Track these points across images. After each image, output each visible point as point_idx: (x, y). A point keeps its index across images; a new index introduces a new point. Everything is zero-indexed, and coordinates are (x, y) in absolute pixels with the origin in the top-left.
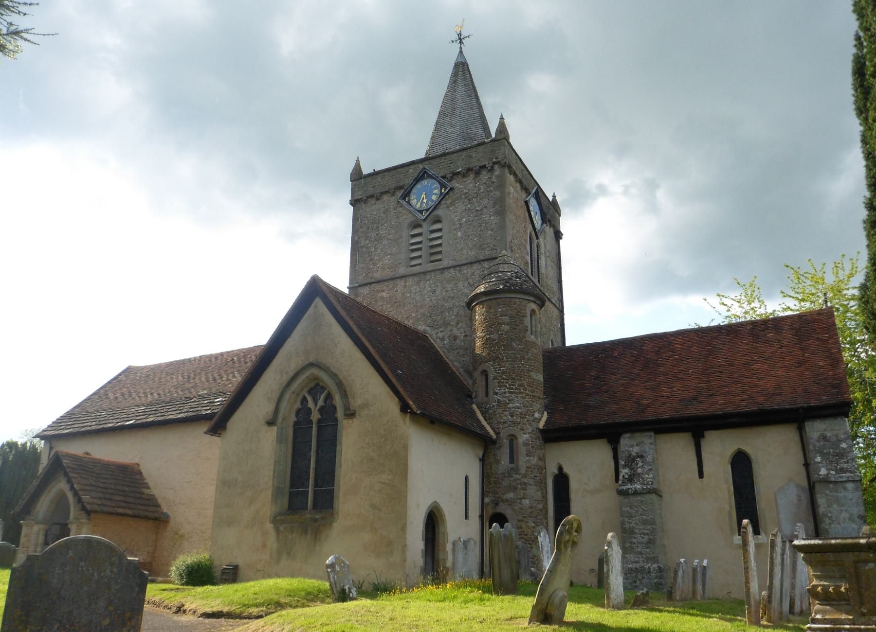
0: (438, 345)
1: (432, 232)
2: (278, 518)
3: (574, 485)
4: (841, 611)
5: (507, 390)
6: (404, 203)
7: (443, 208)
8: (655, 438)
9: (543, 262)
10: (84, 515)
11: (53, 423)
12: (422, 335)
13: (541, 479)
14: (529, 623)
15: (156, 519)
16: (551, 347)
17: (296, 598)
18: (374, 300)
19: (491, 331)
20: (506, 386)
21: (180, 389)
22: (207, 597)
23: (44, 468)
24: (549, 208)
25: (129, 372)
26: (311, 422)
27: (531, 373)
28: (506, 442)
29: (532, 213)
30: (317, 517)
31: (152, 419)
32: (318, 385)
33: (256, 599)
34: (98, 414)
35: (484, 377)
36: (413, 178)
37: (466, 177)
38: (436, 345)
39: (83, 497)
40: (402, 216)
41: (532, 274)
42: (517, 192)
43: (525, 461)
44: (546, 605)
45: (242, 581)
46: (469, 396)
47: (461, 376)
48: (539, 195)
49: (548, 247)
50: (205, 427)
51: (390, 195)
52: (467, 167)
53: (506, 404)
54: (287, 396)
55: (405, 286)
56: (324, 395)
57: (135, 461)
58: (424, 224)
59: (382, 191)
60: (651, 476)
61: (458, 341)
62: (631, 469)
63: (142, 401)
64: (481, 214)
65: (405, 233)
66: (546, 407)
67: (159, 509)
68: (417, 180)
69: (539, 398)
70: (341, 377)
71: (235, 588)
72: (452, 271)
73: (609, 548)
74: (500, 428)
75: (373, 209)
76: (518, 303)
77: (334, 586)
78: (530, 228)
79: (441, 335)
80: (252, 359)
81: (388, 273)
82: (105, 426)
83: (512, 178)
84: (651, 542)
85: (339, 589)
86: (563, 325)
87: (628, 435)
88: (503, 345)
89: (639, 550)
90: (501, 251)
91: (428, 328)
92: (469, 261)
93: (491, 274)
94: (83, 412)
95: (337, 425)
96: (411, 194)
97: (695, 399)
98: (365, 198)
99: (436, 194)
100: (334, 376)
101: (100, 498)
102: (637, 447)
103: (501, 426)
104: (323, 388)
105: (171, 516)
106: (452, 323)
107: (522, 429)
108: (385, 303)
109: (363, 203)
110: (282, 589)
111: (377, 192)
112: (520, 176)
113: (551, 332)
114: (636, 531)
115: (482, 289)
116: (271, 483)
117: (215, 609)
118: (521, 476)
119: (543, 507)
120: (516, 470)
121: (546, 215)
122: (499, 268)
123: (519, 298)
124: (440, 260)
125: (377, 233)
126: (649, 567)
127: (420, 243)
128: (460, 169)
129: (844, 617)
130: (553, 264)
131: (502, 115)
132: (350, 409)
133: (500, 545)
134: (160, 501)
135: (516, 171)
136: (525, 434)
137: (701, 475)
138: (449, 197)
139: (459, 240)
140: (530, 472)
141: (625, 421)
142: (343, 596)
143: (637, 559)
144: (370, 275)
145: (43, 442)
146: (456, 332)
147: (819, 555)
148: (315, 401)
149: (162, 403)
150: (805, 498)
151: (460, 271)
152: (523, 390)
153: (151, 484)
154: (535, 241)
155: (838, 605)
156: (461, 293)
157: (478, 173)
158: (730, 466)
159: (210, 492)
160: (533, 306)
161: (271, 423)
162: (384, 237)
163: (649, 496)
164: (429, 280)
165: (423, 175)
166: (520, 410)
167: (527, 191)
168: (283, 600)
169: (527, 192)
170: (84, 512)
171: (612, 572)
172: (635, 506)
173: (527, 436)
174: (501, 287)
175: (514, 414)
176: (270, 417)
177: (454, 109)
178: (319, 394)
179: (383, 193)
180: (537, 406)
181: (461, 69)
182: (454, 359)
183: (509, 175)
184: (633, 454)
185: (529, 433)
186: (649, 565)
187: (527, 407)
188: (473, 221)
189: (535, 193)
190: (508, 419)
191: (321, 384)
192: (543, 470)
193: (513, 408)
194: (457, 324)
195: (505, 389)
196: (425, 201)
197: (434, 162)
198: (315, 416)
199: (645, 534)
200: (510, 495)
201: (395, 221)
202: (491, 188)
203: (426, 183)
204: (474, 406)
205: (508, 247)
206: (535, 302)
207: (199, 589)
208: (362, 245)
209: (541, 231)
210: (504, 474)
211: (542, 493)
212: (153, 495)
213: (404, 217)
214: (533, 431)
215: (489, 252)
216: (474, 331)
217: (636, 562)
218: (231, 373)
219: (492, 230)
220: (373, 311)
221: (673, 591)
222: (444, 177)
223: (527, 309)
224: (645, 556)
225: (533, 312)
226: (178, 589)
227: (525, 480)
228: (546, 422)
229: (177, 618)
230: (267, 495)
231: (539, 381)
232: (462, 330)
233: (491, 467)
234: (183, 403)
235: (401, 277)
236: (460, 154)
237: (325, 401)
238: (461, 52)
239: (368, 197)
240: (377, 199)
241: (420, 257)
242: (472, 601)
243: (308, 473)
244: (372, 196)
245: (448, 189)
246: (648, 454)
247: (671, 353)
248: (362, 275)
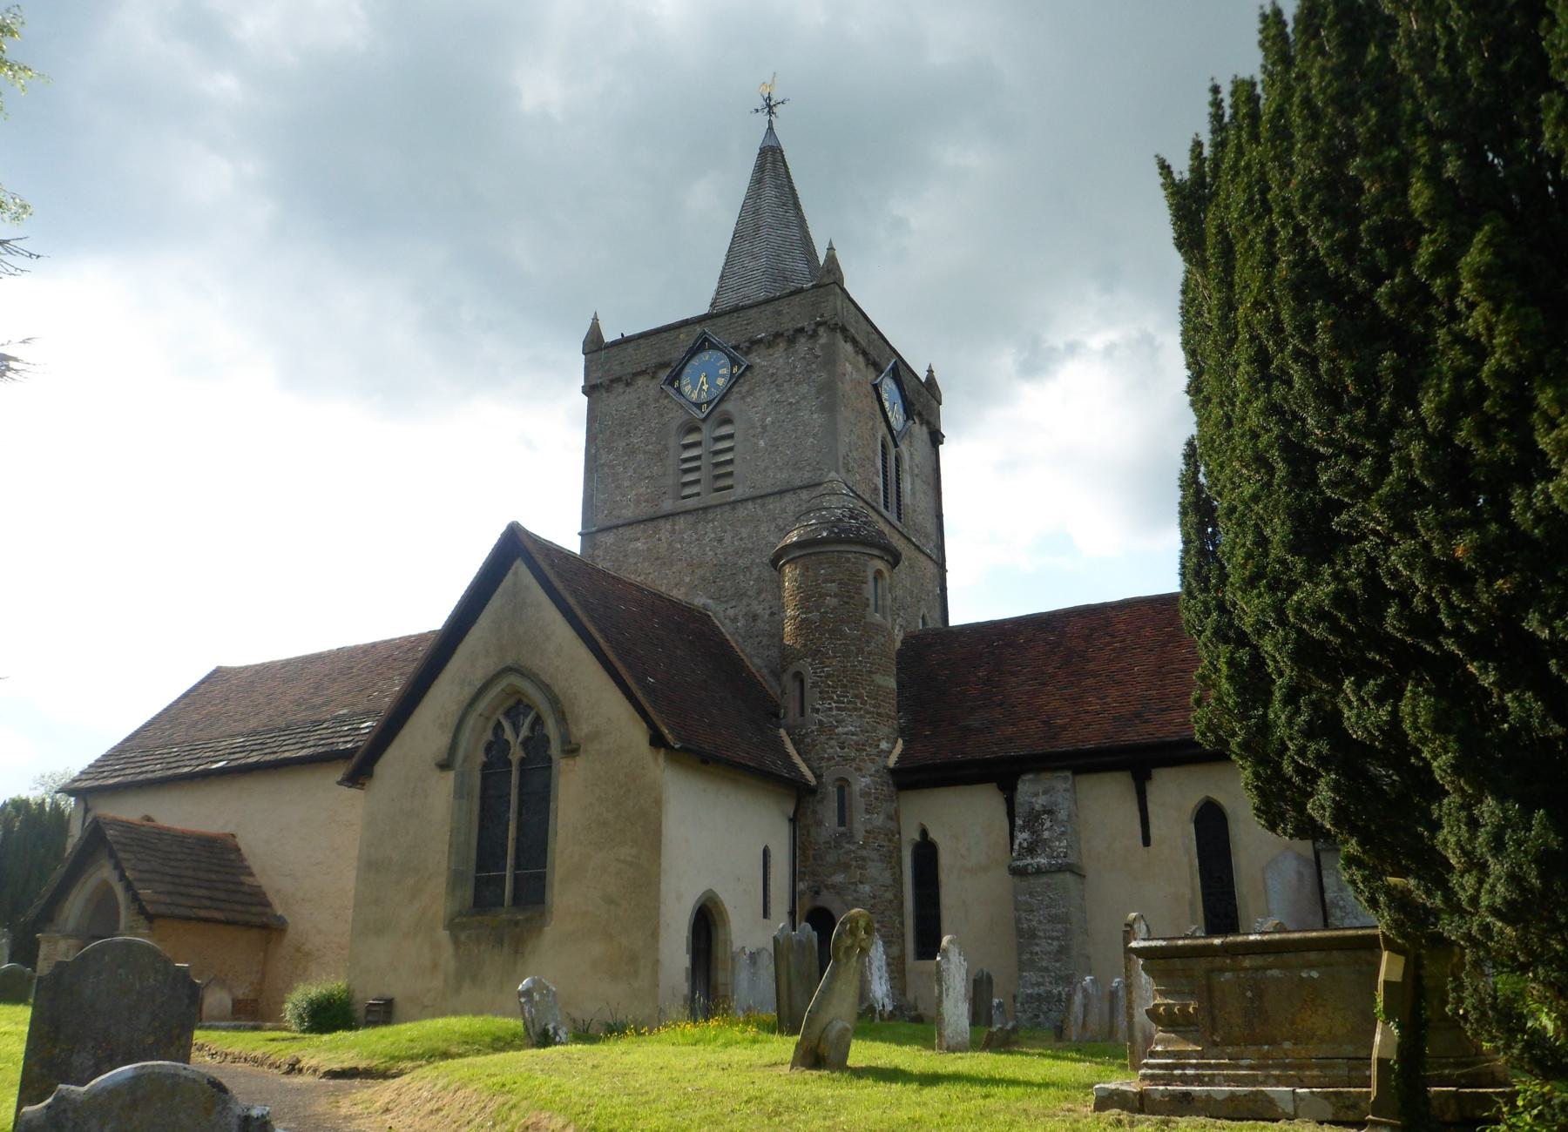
0: (726, 630)
3: (945, 860)
4: (1188, 1040)
5: (834, 705)
6: (672, 392)
9: (906, 485)
10: (142, 920)
11: (90, 766)
12: (700, 613)
13: (890, 851)
14: (791, 1069)
15: (264, 927)
17: (477, 1046)
19: (807, 608)
20: (832, 698)
21: (303, 707)
22: (337, 1048)
23: (75, 846)
24: (919, 394)
25: (218, 676)
26: (509, 763)
28: (832, 790)
29: (887, 405)
30: (520, 917)
31: (255, 759)
32: (519, 702)
33: (412, 1048)
34: (165, 751)
36: (687, 349)
38: (723, 630)
39: (141, 891)
40: (667, 414)
41: (886, 507)
42: (858, 370)
44: (816, 1042)
45: (400, 1022)
46: (773, 713)
47: (765, 680)
48: (900, 371)
49: (918, 459)
50: (339, 772)
51: (647, 377)
54: (471, 721)
55: (673, 532)
56: (530, 718)
57: (227, 830)
58: (704, 427)
61: (759, 623)
62: (1033, 833)
63: (240, 727)
65: (673, 442)
66: (902, 732)
67: (268, 910)
68: (693, 352)
69: (889, 717)
70: (556, 690)
71: (381, 1033)
72: (750, 505)
73: (942, 958)
75: (620, 401)
77: (530, 1026)
78: (882, 430)
79: (731, 612)
82: (177, 771)
83: (849, 347)
84: (1063, 951)
85: (537, 1028)
86: (944, 589)
87: (1031, 776)
90: (829, 471)
91: (710, 601)
92: (776, 490)
93: (809, 512)
94: (140, 747)
95: (551, 767)
96: (683, 377)
97: (1138, 715)
99: (723, 376)
100: (546, 688)
101: (169, 893)
104: (529, 708)
105: (289, 920)
106: (749, 593)
107: (859, 769)
109: (603, 391)
110: (455, 1033)
112: (863, 342)
113: (923, 603)
115: (793, 537)
116: (444, 865)
117: (346, 1065)
119: (895, 896)
120: (849, 837)
121: (913, 404)
122: (822, 502)
123: (855, 552)
124: (730, 487)
126: (1060, 993)
127: (698, 458)
129: (1191, 1047)
130: (925, 487)
131: (831, 243)
132: (570, 742)
133: (791, 958)
134: (271, 897)
135: (856, 335)
136: (864, 777)
137: (1146, 841)
140: (871, 840)
142: (544, 1039)
145: (72, 799)
146: (757, 608)
147: (1162, 961)
148: (516, 729)
149: (272, 731)
150: (1309, 873)
153: (255, 869)
154: (892, 452)
155: (1186, 1032)
157: (791, 341)
158: (1192, 826)
159: (348, 879)
160: (880, 565)
161: (444, 766)
162: (638, 449)
163: (1059, 877)
164: (713, 520)
166: (854, 737)
167: (878, 368)
168: (454, 1050)
170: (142, 917)
171: (947, 995)
172: (1037, 892)
173: (867, 780)
174: (825, 534)
177: (757, 228)
178: (522, 717)
179: (637, 374)
180: (884, 730)
181: (771, 161)
184: (1037, 807)
185: (871, 776)
186: (1060, 989)
188: (783, 421)
189: (892, 369)
191: (525, 700)
193: (846, 734)
194: (759, 593)
196: (705, 387)
197: (721, 322)
198: (516, 754)
199: (1053, 939)
200: (839, 878)
202: (814, 366)
203: (707, 358)
204: (782, 732)
205: (841, 463)
206: (881, 558)
207: (326, 1037)
208: (602, 461)
209: (903, 433)
210: (828, 843)
211: (894, 874)
212: (260, 887)
214: (877, 771)
215: (810, 475)
216: (782, 607)
217: (1039, 984)
218: (390, 678)
219: (815, 435)
220: (614, 578)
221: (1065, 1026)
222: (736, 348)
223: (868, 570)
224: (1053, 974)
225: (878, 574)
226: (294, 1038)
227: (864, 853)
228: (901, 757)
229: (286, 1080)
230: (439, 885)
231: (888, 688)
233: (808, 832)
234: (309, 731)
235: (666, 516)
236: (763, 308)
237: (532, 728)
238: (771, 128)
239: (612, 381)
240: (628, 384)
241: (697, 482)
242: (737, 1043)
244: (619, 380)
245: (743, 368)
246: (1060, 807)
247: (1108, 639)
248: (603, 511)
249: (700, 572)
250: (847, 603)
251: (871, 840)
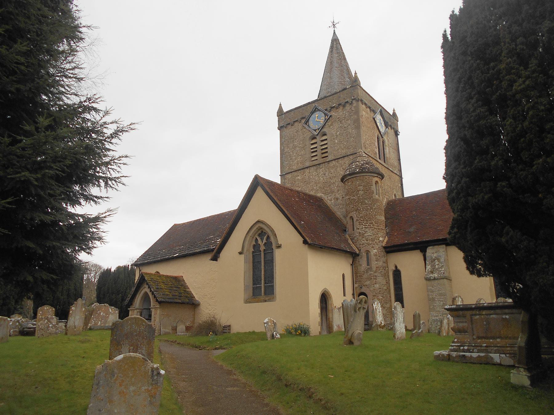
0: (329, 203)
1: (322, 141)
2: (248, 301)
6: (306, 126)
8: (446, 248)
9: (387, 151)
16: (394, 198)
20: (363, 225)
24: (390, 119)
28: (364, 254)
32: (262, 232)
35: (352, 220)
41: (380, 159)
42: (367, 113)
43: (375, 264)
48: (383, 112)
50: (210, 256)
53: (363, 234)
56: (266, 236)
59: (294, 121)
61: (339, 201)
64: (347, 129)
65: (308, 142)
68: (312, 113)
69: (382, 229)
72: (334, 162)
75: (290, 131)
79: (330, 198)
83: (364, 106)
86: (402, 185)
87: (431, 247)
89: (438, 309)
90: (359, 149)
91: (323, 195)
93: (352, 163)
96: (310, 121)
102: (436, 254)
103: (361, 246)
107: (373, 247)
108: (300, 183)
111: (291, 121)
112: (369, 104)
113: (394, 190)
118: (373, 272)
120: (370, 269)
123: (368, 176)
127: (316, 147)
128: (335, 105)
130: (394, 150)
136: (375, 249)
138: (330, 121)
139: (336, 145)
140: (378, 270)
141: (429, 239)
143: (437, 315)
144: (291, 168)
146: (338, 196)
151: (338, 162)
152: (373, 226)
154: (381, 140)
156: (339, 174)
157: (344, 106)
164: (322, 168)
165: (316, 110)
166: (371, 237)
167: (374, 112)
169: (374, 113)
173: (376, 251)
175: (368, 239)
176: (240, 250)
182: (337, 210)
183: (361, 105)
185: (377, 249)
187: (375, 235)
190: (365, 242)
192: (386, 268)
195: (362, 226)
198: (262, 248)
199: (441, 301)
200: (368, 283)
201: (302, 136)
202: (352, 114)
206: (378, 177)
217: (437, 316)
227: (376, 274)
232: (341, 195)
237: (267, 240)
238: (334, 33)
239: (287, 125)
240: (292, 125)
244: (289, 124)
245: (329, 116)
249: (319, 185)
250: (366, 193)
251: (378, 270)
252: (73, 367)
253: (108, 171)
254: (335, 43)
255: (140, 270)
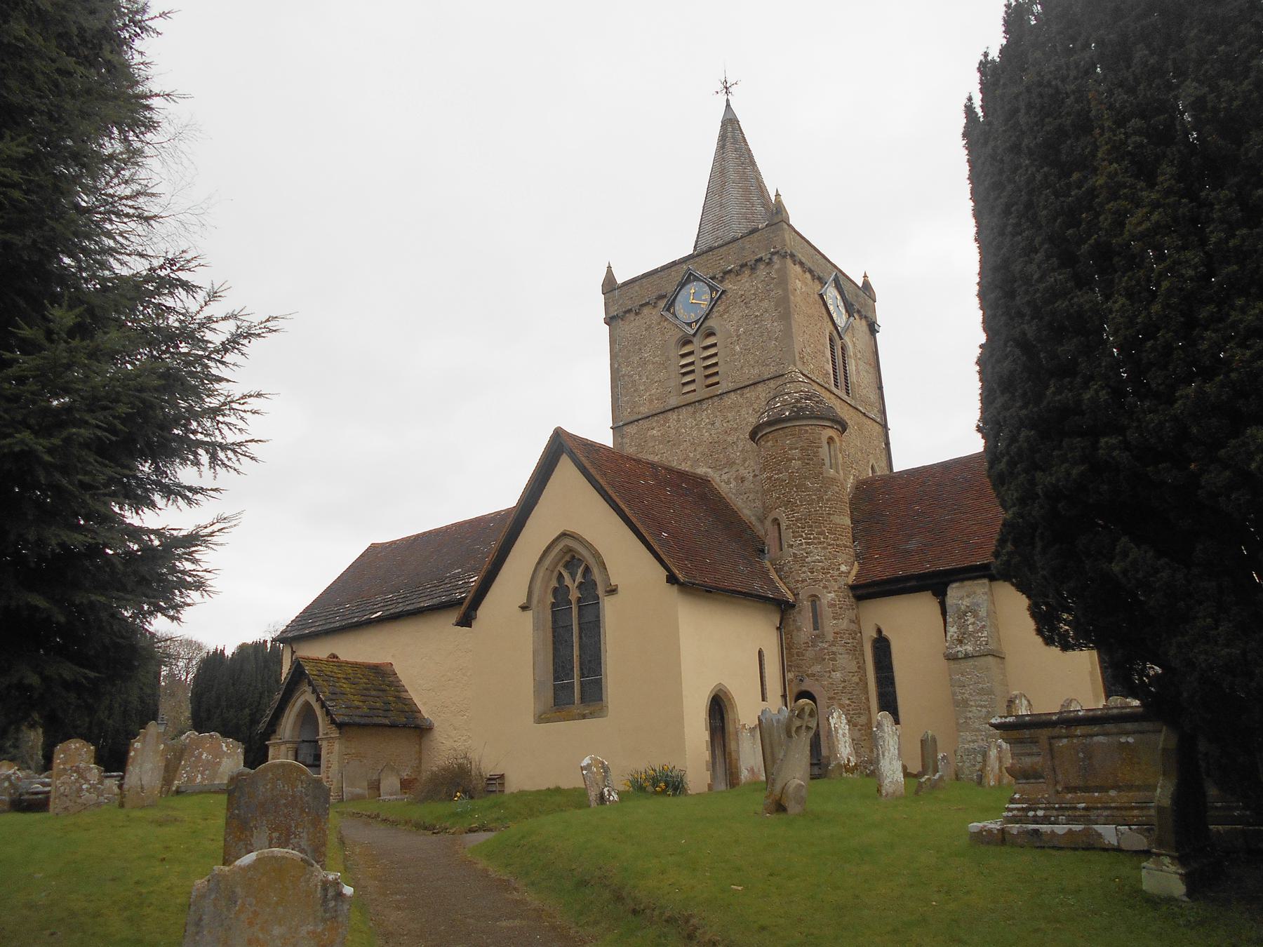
0: (724, 489)
1: (706, 348)
2: (543, 717)
6: (669, 316)
7: (716, 317)
8: (991, 586)
9: (852, 367)
16: (871, 475)
18: (644, 440)
20: (802, 536)
24: (857, 296)
27: (831, 517)
28: (807, 604)
37: (740, 275)
41: (836, 386)
48: (841, 280)
50: (454, 616)
51: (651, 307)
52: (741, 263)
53: (803, 559)
54: (541, 574)
55: (679, 420)
56: (581, 568)
60: (985, 634)
61: (746, 483)
68: (682, 285)
69: (846, 546)
74: (797, 588)
75: (632, 326)
76: (810, 431)
79: (725, 477)
80: (509, 521)
81: (658, 406)
83: (798, 268)
86: (887, 444)
88: (796, 486)
96: (676, 304)
98: (622, 314)
102: (967, 600)
114: (971, 703)
118: (828, 644)
119: (860, 680)
120: (821, 637)
123: (812, 425)
124: (718, 383)
125: (640, 356)
127: (692, 363)
130: (868, 367)
136: (830, 593)
138: (722, 303)
143: (975, 738)
146: (743, 472)
154: (839, 343)
157: (753, 269)
160: (830, 432)
165: (689, 278)
167: (822, 282)
169: (821, 283)
171: (884, 755)
182: (743, 506)
183: (793, 265)
185: (834, 591)
195: (801, 540)
198: (574, 595)
200: (817, 668)
206: (832, 427)
213: (670, 334)
217: (974, 741)
221: (983, 775)
225: (831, 440)
227: (834, 649)
237: (584, 576)
238: (728, 105)
239: (626, 312)
240: (637, 314)
243: (571, 661)
244: (629, 311)
245: (720, 293)
252: (137, 883)
253: (218, 429)
254: (731, 130)
255: (293, 652)
